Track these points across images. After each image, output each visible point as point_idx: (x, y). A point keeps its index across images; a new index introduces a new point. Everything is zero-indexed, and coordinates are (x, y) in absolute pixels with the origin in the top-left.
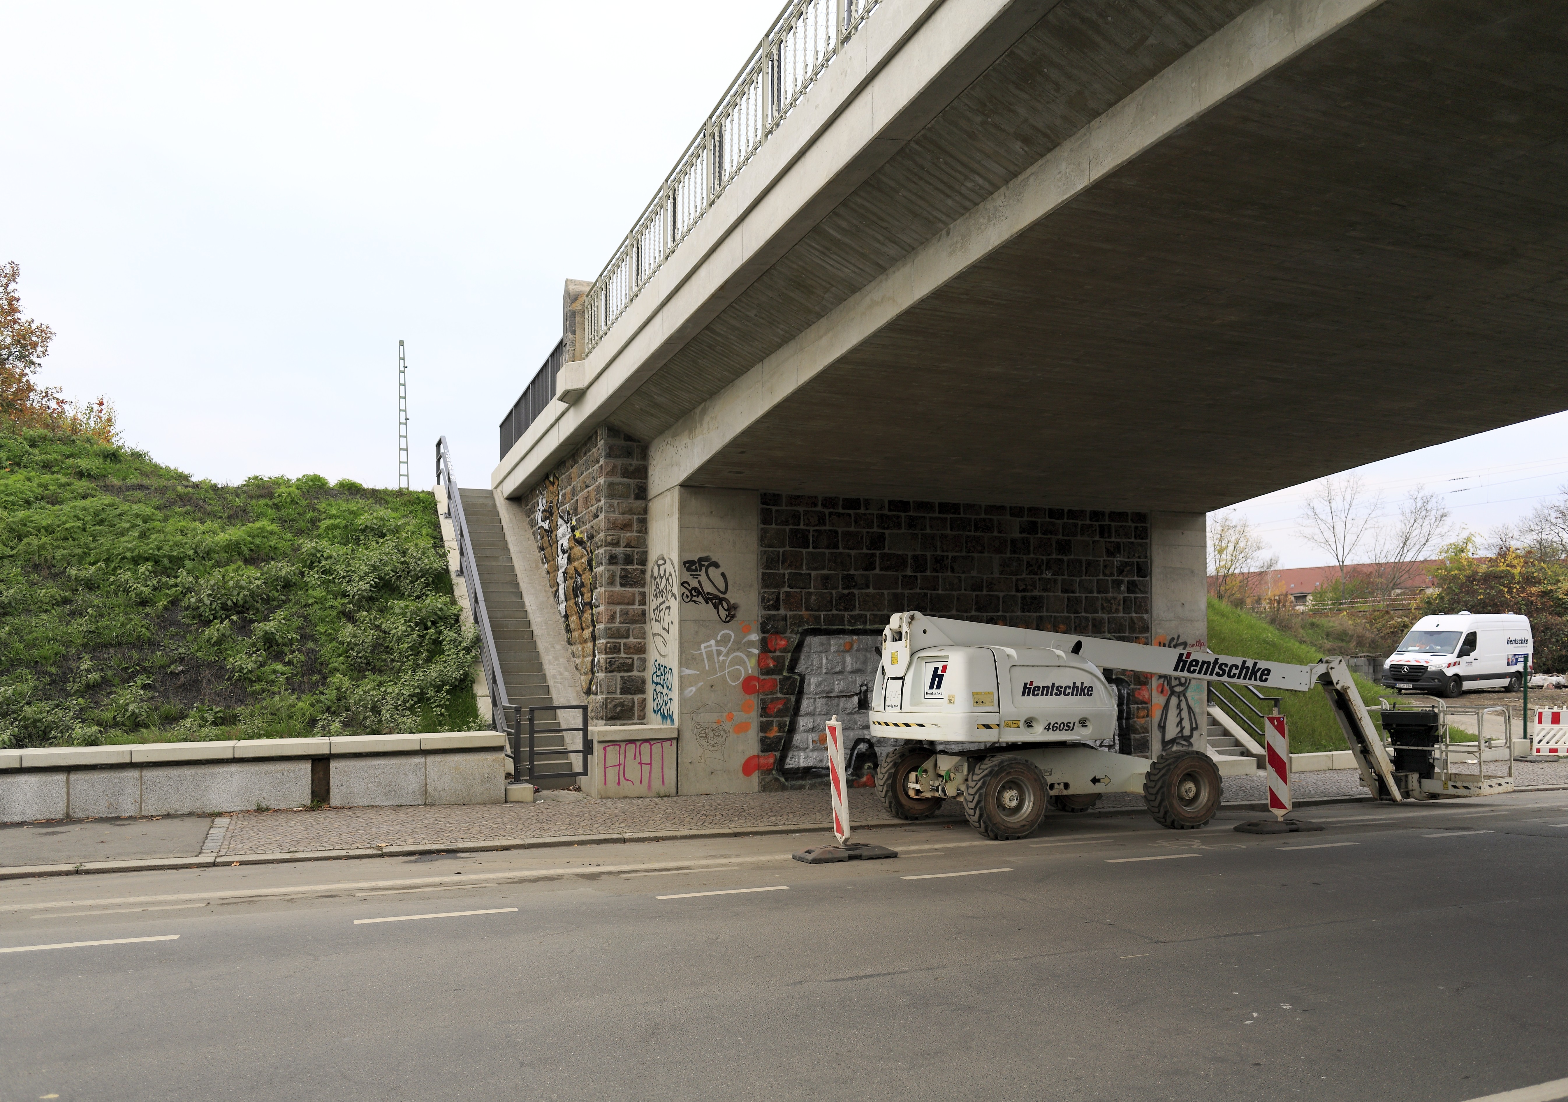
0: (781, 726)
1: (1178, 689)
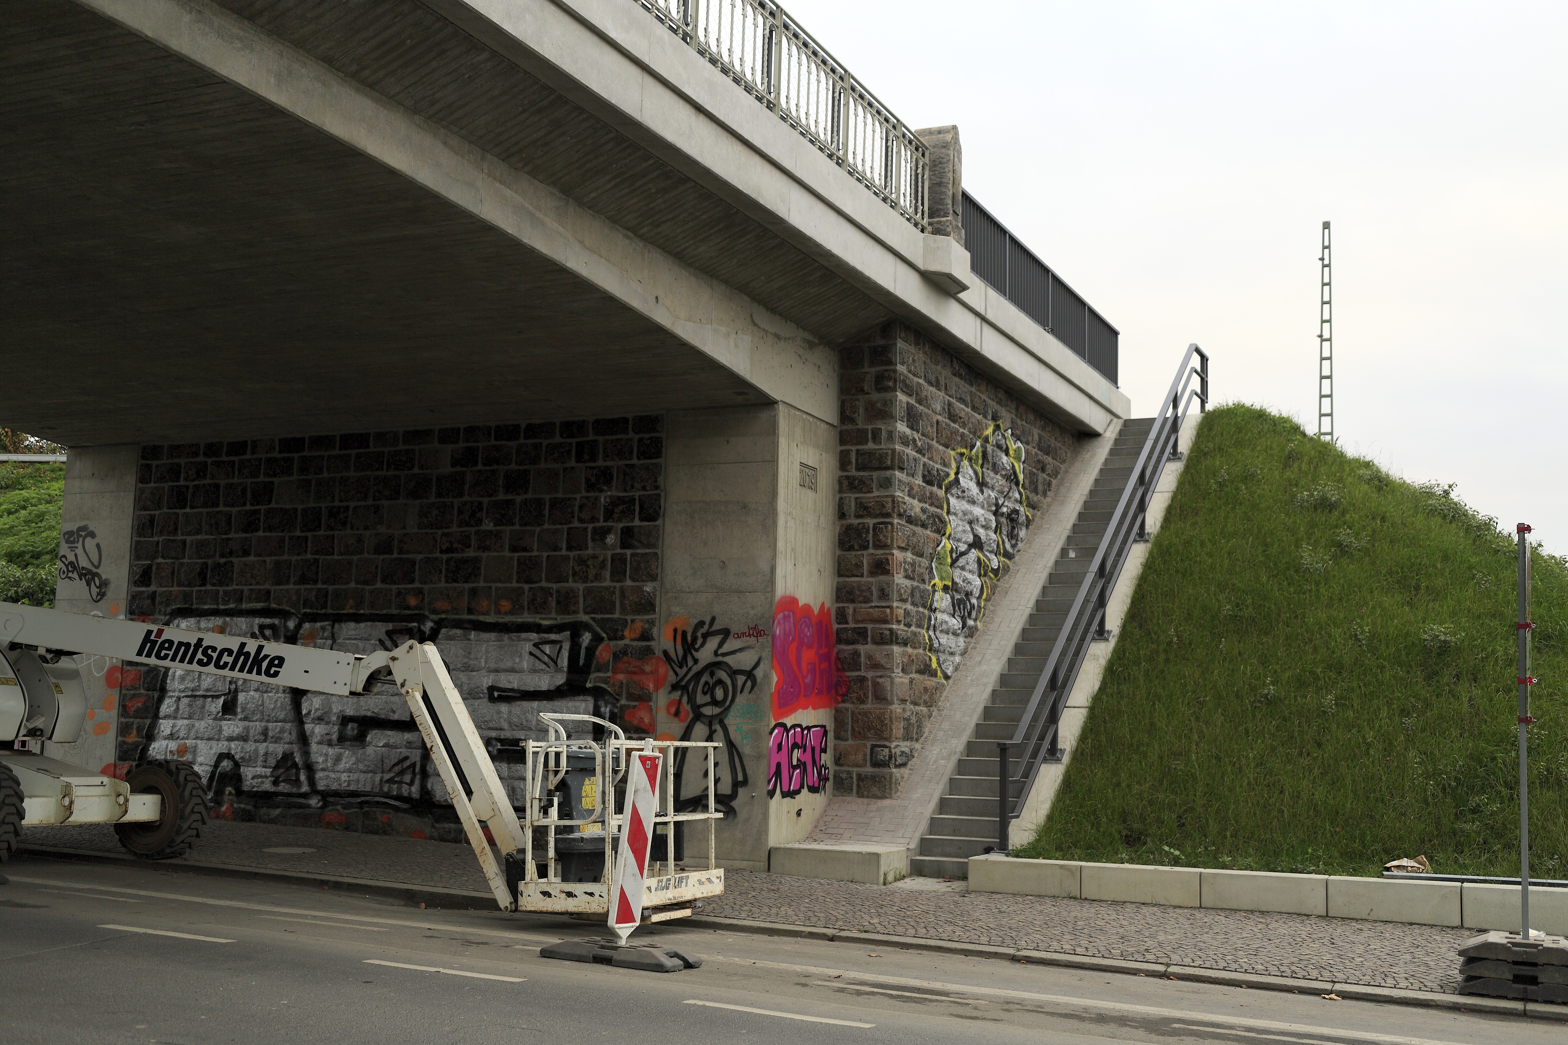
0: (139, 729)
1: (708, 711)
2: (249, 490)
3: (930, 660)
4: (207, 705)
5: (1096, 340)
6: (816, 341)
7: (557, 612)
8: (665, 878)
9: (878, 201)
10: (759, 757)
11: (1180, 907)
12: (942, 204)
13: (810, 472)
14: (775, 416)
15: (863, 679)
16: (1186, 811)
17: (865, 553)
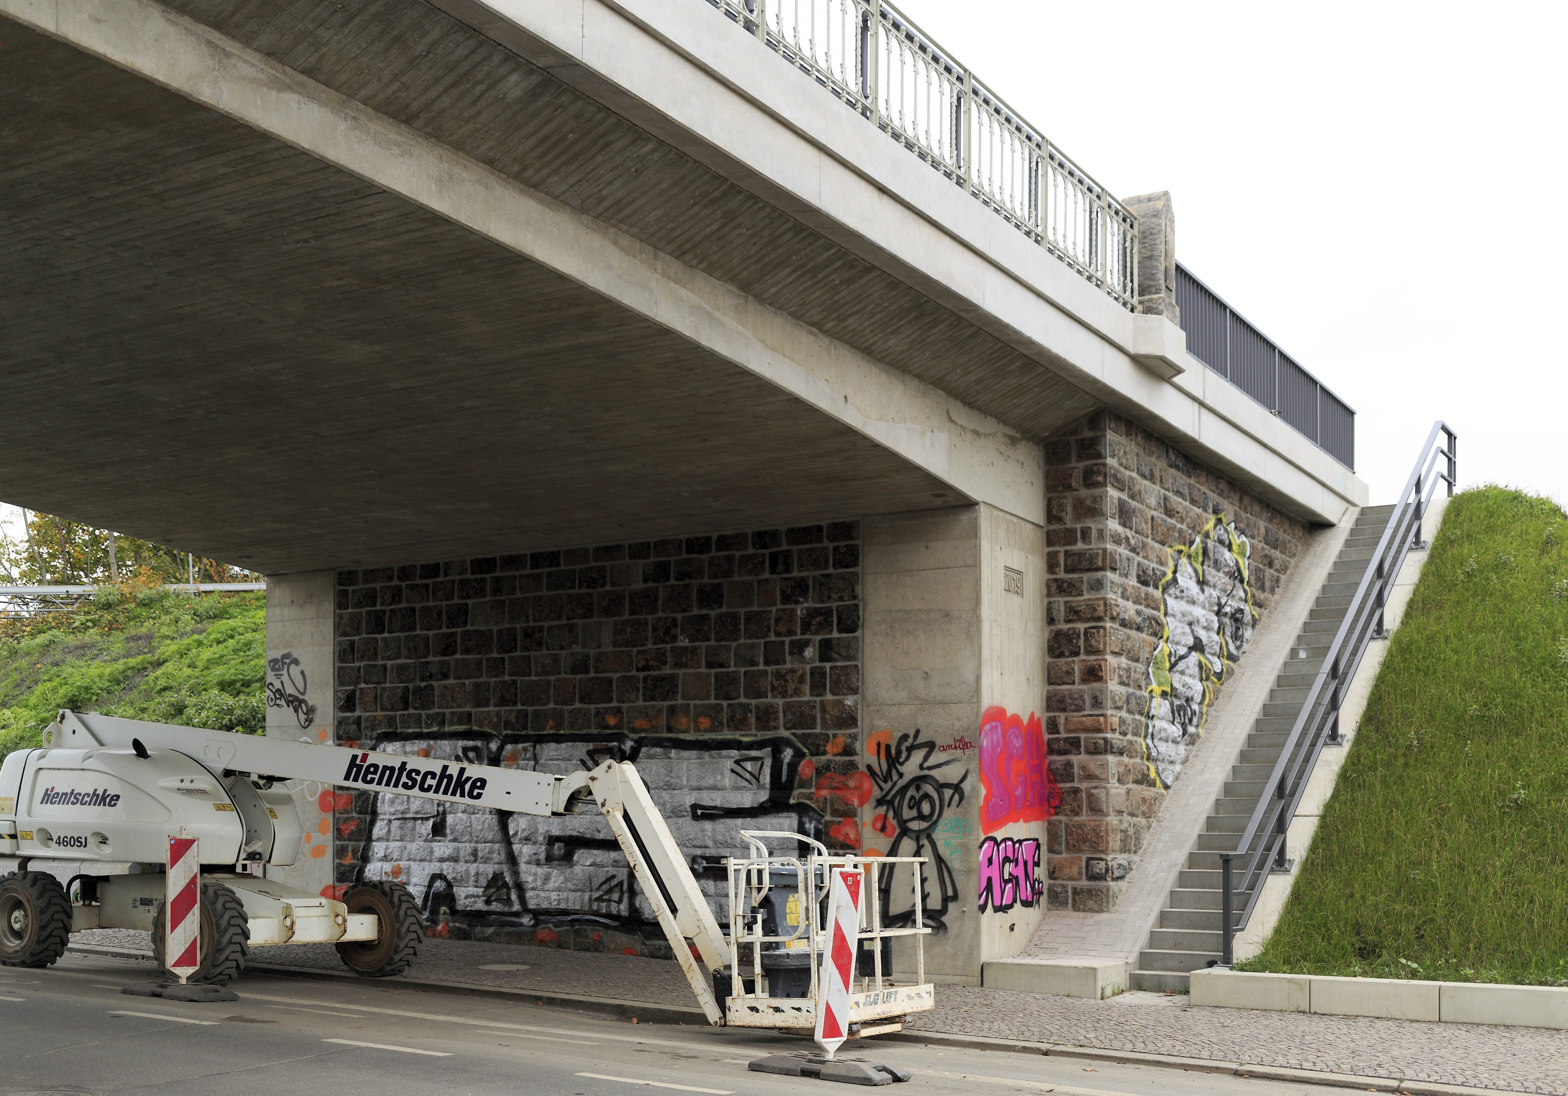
0: (355, 852)
1: (915, 826)
2: (444, 613)
3: (1148, 769)
4: (418, 827)
5: (1328, 421)
6: (1019, 436)
7: (758, 729)
8: (873, 994)
9: (1082, 280)
10: (969, 871)
11: (1417, 1021)
12: (1154, 280)
13: (1016, 576)
14: (976, 518)
15: (1076, 791)
16: (1425, 922)
17: (1076, 659)
